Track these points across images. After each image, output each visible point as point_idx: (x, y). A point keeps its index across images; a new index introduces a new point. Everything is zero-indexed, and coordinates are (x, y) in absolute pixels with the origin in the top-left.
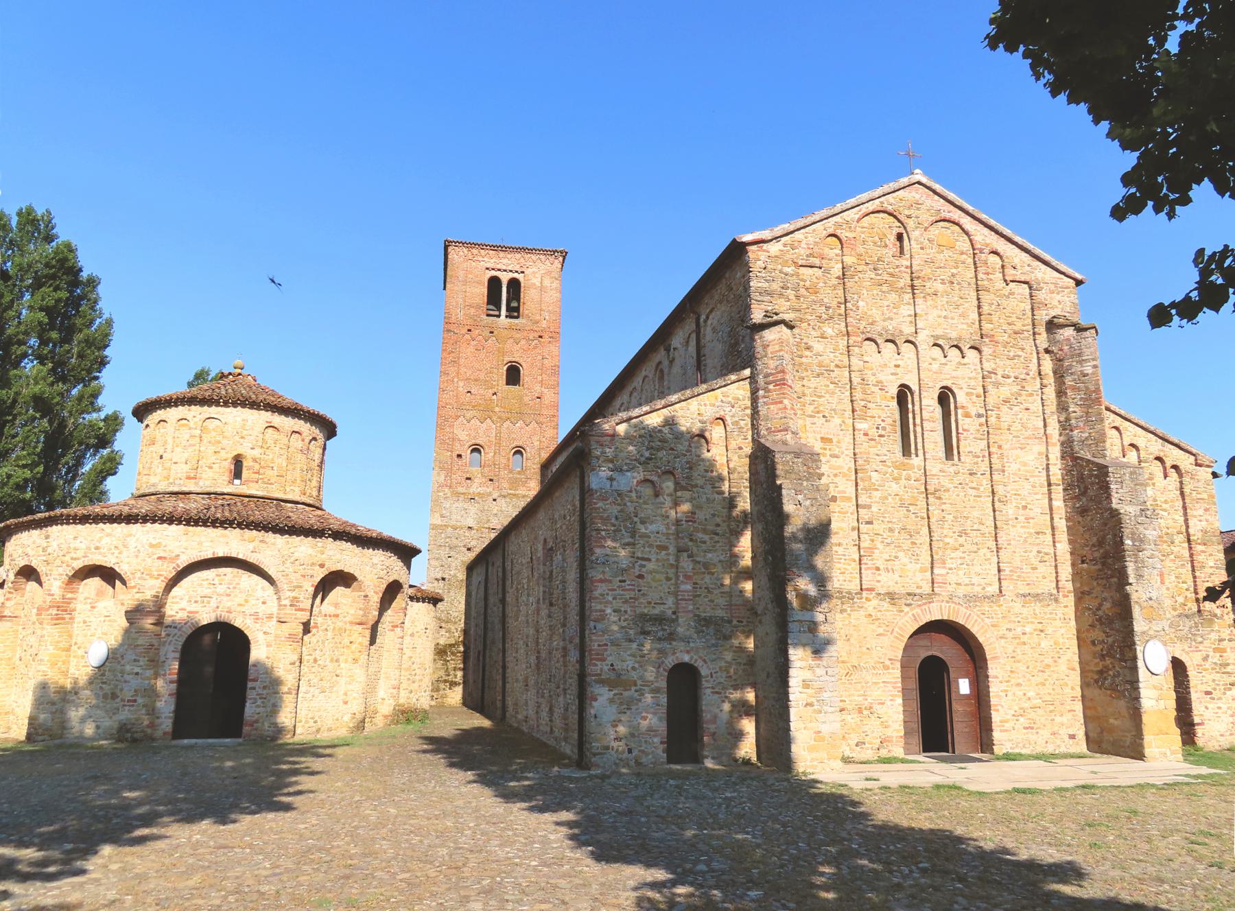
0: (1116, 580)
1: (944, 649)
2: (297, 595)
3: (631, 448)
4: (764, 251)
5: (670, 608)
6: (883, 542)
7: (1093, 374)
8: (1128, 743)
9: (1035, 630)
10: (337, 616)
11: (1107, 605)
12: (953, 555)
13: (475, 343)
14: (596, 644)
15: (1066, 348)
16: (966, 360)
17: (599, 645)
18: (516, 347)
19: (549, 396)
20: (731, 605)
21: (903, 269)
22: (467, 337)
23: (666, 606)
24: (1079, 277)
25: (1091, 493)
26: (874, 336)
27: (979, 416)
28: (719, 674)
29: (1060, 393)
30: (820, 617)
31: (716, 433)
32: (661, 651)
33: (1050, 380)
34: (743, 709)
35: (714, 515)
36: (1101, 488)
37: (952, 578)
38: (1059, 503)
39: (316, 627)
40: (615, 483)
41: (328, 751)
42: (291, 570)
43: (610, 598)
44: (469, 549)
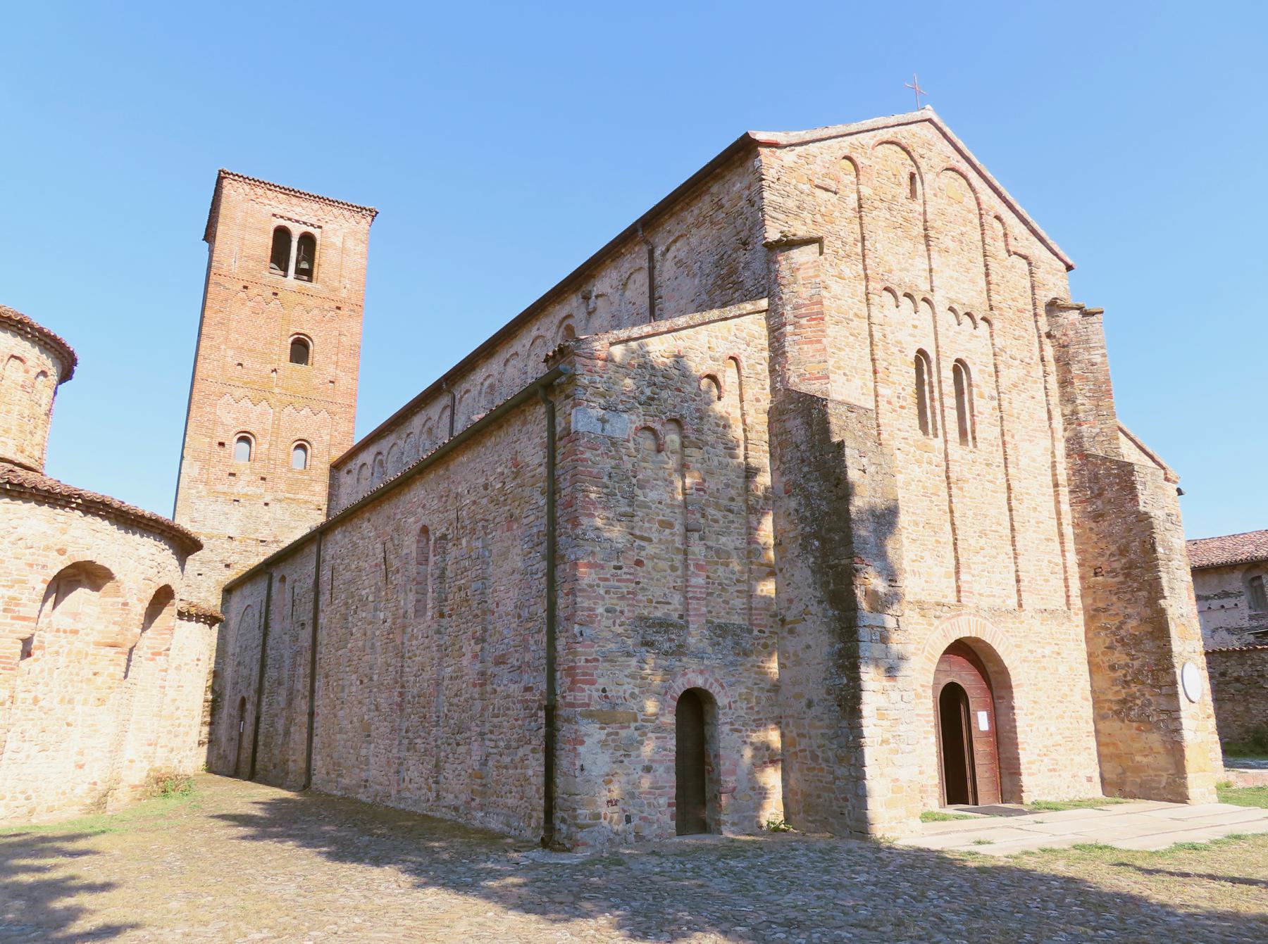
0: (1144, 593)
1: (967, 678)
2: (16, 595)
3: (628, 381)
4: (777, 158)
5: (676, 610)
6: (908, 538)
7: (1102, 363)
9: (1053, 652)
10: (75, 632)
11: (1132, 623)
13: (251, 304)
14: (583, 658)
15: (1071, 333)
16: (977, 332)
17: (587, 661)
18: (306, 316)
19: (344, 381)
20: (751, 609)
21: (916, 215)
22: (242, 295)
23: (671, 607)
24: (1070, 262)
25: (1108, 494)
26: (893, 287)
27: (992, 398)
28: (738, 704)
29: (1064, 383)
30: (890, 623)
31: (729, 377)
32: (668, 671)
33: (1052, 367)
34: (765, 756)
35: (727, 485)
36: (1122, 489)
38: (1065, 507)
39: (41, 648)
40: (607, 426)
41: (81, 845)
42: (9, 554)
43: (602, 592)
44: (227, 566)
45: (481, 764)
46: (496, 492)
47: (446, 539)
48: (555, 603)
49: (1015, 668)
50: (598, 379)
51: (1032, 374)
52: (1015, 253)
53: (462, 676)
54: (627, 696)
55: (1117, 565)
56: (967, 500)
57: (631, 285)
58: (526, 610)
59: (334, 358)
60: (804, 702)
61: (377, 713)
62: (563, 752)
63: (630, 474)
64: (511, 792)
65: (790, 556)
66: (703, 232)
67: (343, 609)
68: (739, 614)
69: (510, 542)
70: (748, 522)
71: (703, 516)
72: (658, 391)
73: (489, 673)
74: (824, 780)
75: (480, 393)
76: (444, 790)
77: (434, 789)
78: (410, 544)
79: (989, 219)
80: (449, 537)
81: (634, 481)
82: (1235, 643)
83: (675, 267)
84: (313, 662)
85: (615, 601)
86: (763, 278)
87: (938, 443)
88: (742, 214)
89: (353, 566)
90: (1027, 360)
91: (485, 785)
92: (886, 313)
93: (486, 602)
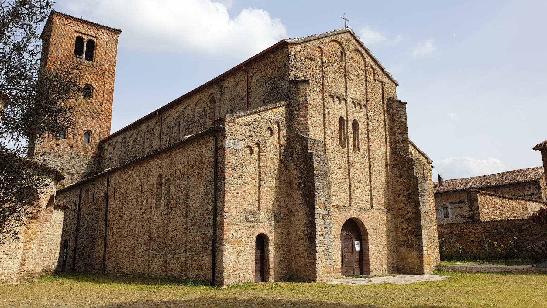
8: (416, 269)
12: (357, 191)
15: (395, 111)
16: (362, 110)
17: (227, 224)
20: (281, 207)
23: (255, 206)
27: (366, 134)
37: (357, 201)
40: (235, 146)
45: (185, 261)
46: (192, 165)
47: (170, 180)
48: (217, 205)
49: (369, 229)
50: (233, 129)
51: (381, 125)
52: (378, 80)
53: (177, 230)
54: (240, 236)
55: (406, 194)
56: (355, 170)
57: (238, 86)
58: (205, 207)
59: (102, 95)
60: (297, 239)
61: (137, 244)
62: (219, 255)
63: (242, 162)
64: (197, 270)
65: (294, 189)
66: (267, 71)
67: (120, 204)
68: (277, 209)
69: (198, 183)
70: (280, 177)
71: (266, 175)
72: (252, 133)
73: (189, 229)
74: (303, 264)
75: (174, 118)
76: (169, 271)
77: (165, 271)
78: (153, 181)
79: (368, 68)
80: (171, 179)
81: (244, 164)
82: (462, 220)
83: (256, 82)
84: (106, 225)
85: (237, 204)
86: (288, 92)
87: (345, 150)
88: (281, 67)
89: (125, 188)
90: (379, 120)
91: (186, 268)
92: (330, 104)
93: (188, 203)
